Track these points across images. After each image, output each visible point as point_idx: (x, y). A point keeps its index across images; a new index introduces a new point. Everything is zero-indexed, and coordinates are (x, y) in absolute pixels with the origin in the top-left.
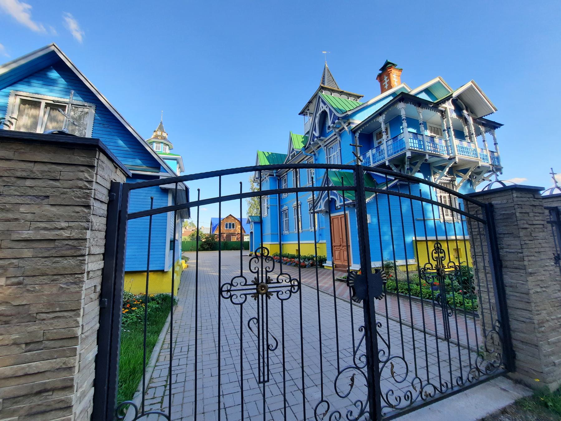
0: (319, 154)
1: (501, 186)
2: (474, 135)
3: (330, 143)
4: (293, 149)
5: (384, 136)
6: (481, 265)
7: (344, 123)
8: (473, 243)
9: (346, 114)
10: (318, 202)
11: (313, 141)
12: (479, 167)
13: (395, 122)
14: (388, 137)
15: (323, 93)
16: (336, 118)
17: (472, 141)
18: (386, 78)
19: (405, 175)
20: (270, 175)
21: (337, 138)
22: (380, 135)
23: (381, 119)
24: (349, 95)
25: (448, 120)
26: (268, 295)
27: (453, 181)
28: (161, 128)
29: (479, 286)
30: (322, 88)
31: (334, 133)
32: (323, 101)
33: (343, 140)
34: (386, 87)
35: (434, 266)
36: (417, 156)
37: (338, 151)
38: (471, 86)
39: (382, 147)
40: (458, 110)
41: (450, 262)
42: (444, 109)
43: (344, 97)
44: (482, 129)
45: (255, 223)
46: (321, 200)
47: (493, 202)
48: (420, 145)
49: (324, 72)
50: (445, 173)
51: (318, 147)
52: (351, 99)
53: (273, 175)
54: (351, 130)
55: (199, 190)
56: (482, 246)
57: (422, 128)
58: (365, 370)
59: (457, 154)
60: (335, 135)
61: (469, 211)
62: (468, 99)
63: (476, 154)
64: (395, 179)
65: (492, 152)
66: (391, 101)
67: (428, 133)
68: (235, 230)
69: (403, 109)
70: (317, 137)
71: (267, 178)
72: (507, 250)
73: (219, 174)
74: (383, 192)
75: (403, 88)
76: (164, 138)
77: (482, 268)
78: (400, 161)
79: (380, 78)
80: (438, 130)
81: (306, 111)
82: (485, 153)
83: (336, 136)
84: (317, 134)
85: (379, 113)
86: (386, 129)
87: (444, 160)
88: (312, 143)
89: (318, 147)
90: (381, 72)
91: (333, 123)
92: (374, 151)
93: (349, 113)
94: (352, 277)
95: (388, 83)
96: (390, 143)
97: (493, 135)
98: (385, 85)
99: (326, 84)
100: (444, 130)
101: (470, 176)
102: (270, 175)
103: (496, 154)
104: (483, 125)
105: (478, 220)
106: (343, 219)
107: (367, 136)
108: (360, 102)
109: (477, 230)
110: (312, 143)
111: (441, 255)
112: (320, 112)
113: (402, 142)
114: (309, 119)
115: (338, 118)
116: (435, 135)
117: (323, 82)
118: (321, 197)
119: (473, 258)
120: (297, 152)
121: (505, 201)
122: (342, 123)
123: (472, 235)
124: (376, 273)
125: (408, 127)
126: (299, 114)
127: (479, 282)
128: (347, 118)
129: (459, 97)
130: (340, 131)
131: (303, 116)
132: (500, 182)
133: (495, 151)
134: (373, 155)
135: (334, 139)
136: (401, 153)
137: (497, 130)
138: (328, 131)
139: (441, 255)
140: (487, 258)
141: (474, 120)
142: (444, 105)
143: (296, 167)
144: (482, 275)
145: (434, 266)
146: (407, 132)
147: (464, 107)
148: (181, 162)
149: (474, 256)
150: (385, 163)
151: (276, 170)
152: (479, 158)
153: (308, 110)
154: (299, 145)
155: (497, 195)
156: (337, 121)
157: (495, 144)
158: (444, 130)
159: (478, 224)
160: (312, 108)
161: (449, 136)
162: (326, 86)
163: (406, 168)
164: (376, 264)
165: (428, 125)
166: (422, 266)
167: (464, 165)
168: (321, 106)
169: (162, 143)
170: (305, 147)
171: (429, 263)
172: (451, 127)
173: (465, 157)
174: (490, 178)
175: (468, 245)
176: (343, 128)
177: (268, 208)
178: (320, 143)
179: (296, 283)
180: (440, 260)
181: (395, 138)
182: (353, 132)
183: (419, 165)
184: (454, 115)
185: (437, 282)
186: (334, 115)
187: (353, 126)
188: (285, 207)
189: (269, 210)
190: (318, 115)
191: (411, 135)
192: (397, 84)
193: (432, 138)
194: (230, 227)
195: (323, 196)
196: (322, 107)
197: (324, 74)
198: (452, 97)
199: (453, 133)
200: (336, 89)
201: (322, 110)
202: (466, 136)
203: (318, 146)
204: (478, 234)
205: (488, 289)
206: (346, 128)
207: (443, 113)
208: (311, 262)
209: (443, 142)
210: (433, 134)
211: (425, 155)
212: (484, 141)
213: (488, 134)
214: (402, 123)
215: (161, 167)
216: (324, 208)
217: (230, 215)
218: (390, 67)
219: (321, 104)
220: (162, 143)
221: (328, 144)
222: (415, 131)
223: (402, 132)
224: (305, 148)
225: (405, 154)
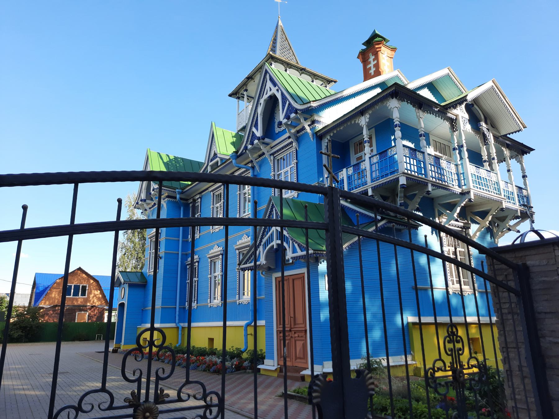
0: (260, 166)
1: (538, 238)
2: (496, 161)
3: (280, 150)
4: (215, 155)
5: (367, 149)
6: (515, 364)
7: (306, 119)
8: (504, 328)
9: (309, 105)
11: (252, 143)
12: (502, 210)
13: (384, 128)
14: (372, 151)
15: (273, 66)
16: (291, 109)
17: (492, 169)
18: (372, 58)
19: (402, 208)
20: (168, 197)
21: (291, 143)
22: (360, 146)
23: (363, 121)
24: (314, 76)
27: (466, 227)
29: (515, 400)
30: (271, 58)
31: (287, 135)
32: (272, 80)
34: (372, 72)
35: (448, 364)
36: (416, 184)
37: (293, 164)
39: (362, 166)
40: (474, 121)
41: (471, 357)
42: (454, 117)
43: (306, 78)
44: (507, 152)
45: (131, 286)
46: (261, 248)
47: (529, 263)
48: (419, 168)
49: (276, 32)
50: (455, 215)
51: (260, 156)
52: (317, 83)
53: (175, 198)
54: (316, 133)
55: (25, 208)
56: (515, 331)
57: (423, 142)
59: (472, 187)
60: (289, 137)
61: (495, 275)
62: (489, 106)
63: (499, 190)
65: (520, 188)
66: (378, 94)
67: (431, 150)
68: (87, 300)
69: (396, 109)
70: (259, 139)
72: (551, 339)
73: (76, 179)
74: (369, 236)
75: (397, 76)
77: (517, 369)
78: (389, 190)
79: (364, 56)
80: (445, 148)
81: (242, 91)
82: (510, 190)
85: (360, 111)
86: (370, 138)
87: (454, 194)
88: (250, 146)
89: (260, 156)
90: (364, 47)
91: (287, 117)
92: (351, 171)
93: (314, 105)
94: (317, 385)
95: (374, 66)
96: (375, 160)
97: (521, 162)
98: (370, 68)
99: (278, 52)
100: (454, 149)
101: (490, 223)
102: (168, 197)
103: (525, 192)
104: (508, 146)
105: (510, 290)
106: (186, 330)
107: (341, 144)
108: (330, 89)
109: (507, 306)
110: (250, 146)
111: (459, 346)
112: (265, 97)
113: (393, 162)
114: (246, 107)
115: (296, 111)
116: (440, 155)
117: (274, 49)
118: (261, 241)
119: (502, 352)
120: (222, 159)
121: (545, 262)
122: (302, 120)
123: (502, 314)
124: (358, 376)
125: (403, 138)
127: (514, 393)
128: (310, 113)
129: (476, 101)
130: (298, 132)
131: (237, 100)
132: (537, 232)
133: (523, 187)
134: (349, 178)
135: (288, 145)
136: (391, 177)
137: (526, 157)
138: (277, 130)
139: (459, 346)
140: (523, 351)
141: (496, 138)
142: (455, 111)
143: (227, 181)
144: (517, 381)
145: (448, 364)
146: (400, 146)
147: (483, 117)
149: (505, 349)
150: (366, 193)
151: (178, 195)
152: (503, 197)
153: (246, 90)
154: (225, 148)
155: (533, 252)
156: (293, 115)
157: (524, 177)
158: (454, 149)
159: (509, 296)
160: (253, 88)
161: (461, 158)
162: (278, 55)
163: (399, 203)
164: (355, 364)
165: (431, 138)
166: (429, 365)
167: (481, 204)
168: (267, 87)
170: (236, 152)
171: (440, 359)
172: (465, 145)
173: (484, 193)
174: (518, 228)
175: (495, 330)
176: (303, 128)
178: (264, 149)
179: (215, 400)
180: (456, 354)
181: (382, 153)
182: (319, 136)
183: (418, 200)
184: (468, 127)
185: (452, 394)
186: (290, 104)
187: (319, 127)
190: (262, 101)
191: (407, 151)
192: (389, 70)
193: (437, 159)
195: (264, 240)
196: (270, 90)
198: (466, 100)
199: (466, 155)
200: (293, 62)
201: (269, 93)
202: (485, 161)
203: (260, 153)
204: (509, 313)
205: (528, 406)
206: (308, 129)
207: (453, 123)
208: (235, 361)
209: (453, 166)
210: (438, 154)
211: (426, 185)
212: (509, 171)
213: (514, 161)
214: (395, 131)
216: (264, 262)
217: (80, 269)
218: (379, 43)
219: (269, 84)
221: (278, 151)
222: (412, 146)
223: (393, 144)
224: (237, 155)
225: (397, 180)
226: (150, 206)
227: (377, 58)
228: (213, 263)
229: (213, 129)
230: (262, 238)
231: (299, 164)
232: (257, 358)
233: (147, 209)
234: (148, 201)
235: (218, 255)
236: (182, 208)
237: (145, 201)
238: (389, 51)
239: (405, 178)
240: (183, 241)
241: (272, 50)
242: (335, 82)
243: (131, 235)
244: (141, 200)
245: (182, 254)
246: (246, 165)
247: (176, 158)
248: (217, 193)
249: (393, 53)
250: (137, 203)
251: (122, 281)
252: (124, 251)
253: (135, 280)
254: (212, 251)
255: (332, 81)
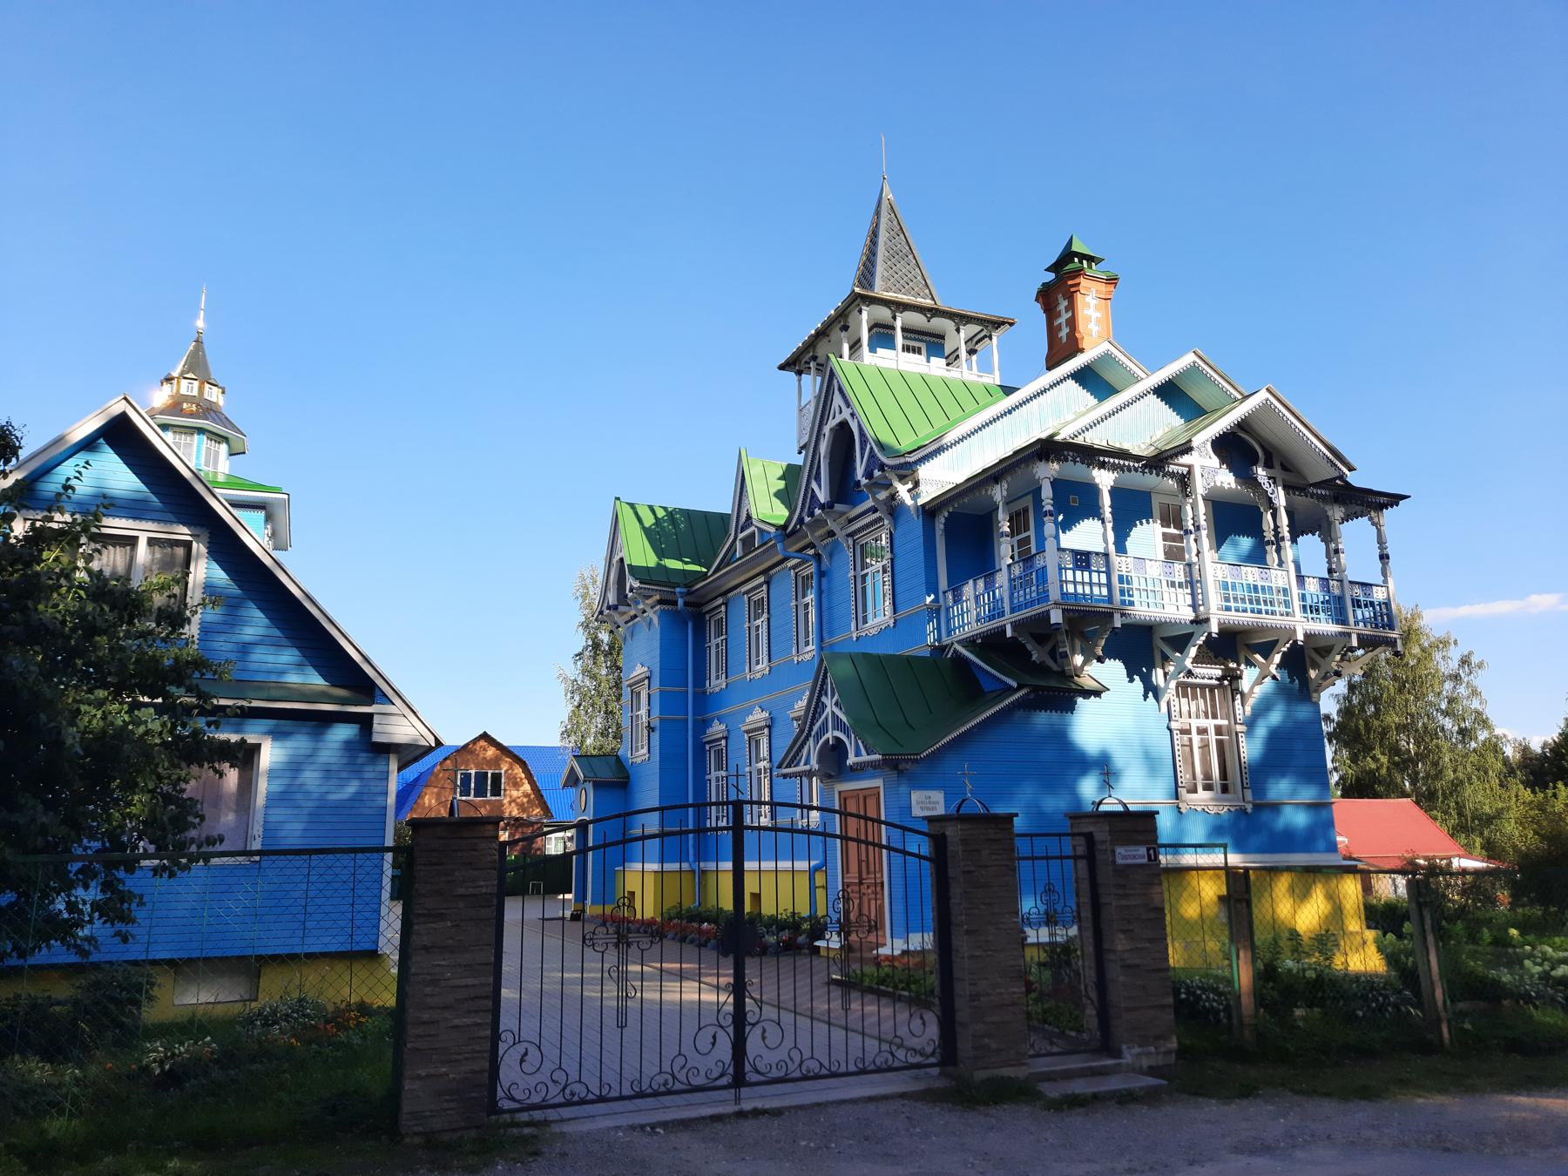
4: (749, 517)
10: (802, 746)
11: (811, 514)
16: (873, 462)
18: (1063, 304)
20: (660, 602)
21: (880, 519)
23: (998, 493)
25: (1195, 501)
26: (629, 945)
28: (197, 365)
33: (899, 530)
38: (1266, 402)
42: (1185, 470)
49: (878, 213)
53: (675, 603)
58: (731, 1030)
60: (875, 510)
64: (1020, 687)
70: (822, 507)
71: (650, 614)
76: (209, 410)
83: (877, 515)
84: (822, 496)
88: (807, 519)
90: (1051, 276)
102: (660, 602)
110: (807, 519)
112: (832, 423)
115: (882, 467)
118: (811, 729)
126: (782, 368)
136: (1038, 609)
148: (280, 515)
156: (877, 473)
157: (1384, 557)
169: (201, 431)
177: (650, 729)
182: (929, 512)
188: (717, 729)
189: (656, 736)
194: (480, 792)
195: (816, 728)
197: (874, 234)
201: (839, 419)
202: (1268, 543)
208: (785, 935)
215: (378, 692)
217: (485, 736)
220: (201, 431)
225: (1047, 615)
226: (626, 618)
227: (1071, 307)
228: (754, 743)
229: (747, 461)
230: (812, 724)
231: (897, 562)
232: (818, 930)
233: (621, 623)
234: (621, 608)
235: (761, 728)
236: (690, 625)
237: (615, 608)
238: (1102, 287)
239: (1060, 612)
240: (695, 694)
241: (861, 285)
242: (1011, 324)
243: (591, 662)
244: (609, 608)
245: (695, 721)
246: (801, 550)
247: (671, 514)
248: (756, 598)
249: (1111, 288)
250: (601, 613)
251: (581, 776)
252: (577, 698)
253: (606, 774)
254: (751, 718)
255: (1003, 323)
